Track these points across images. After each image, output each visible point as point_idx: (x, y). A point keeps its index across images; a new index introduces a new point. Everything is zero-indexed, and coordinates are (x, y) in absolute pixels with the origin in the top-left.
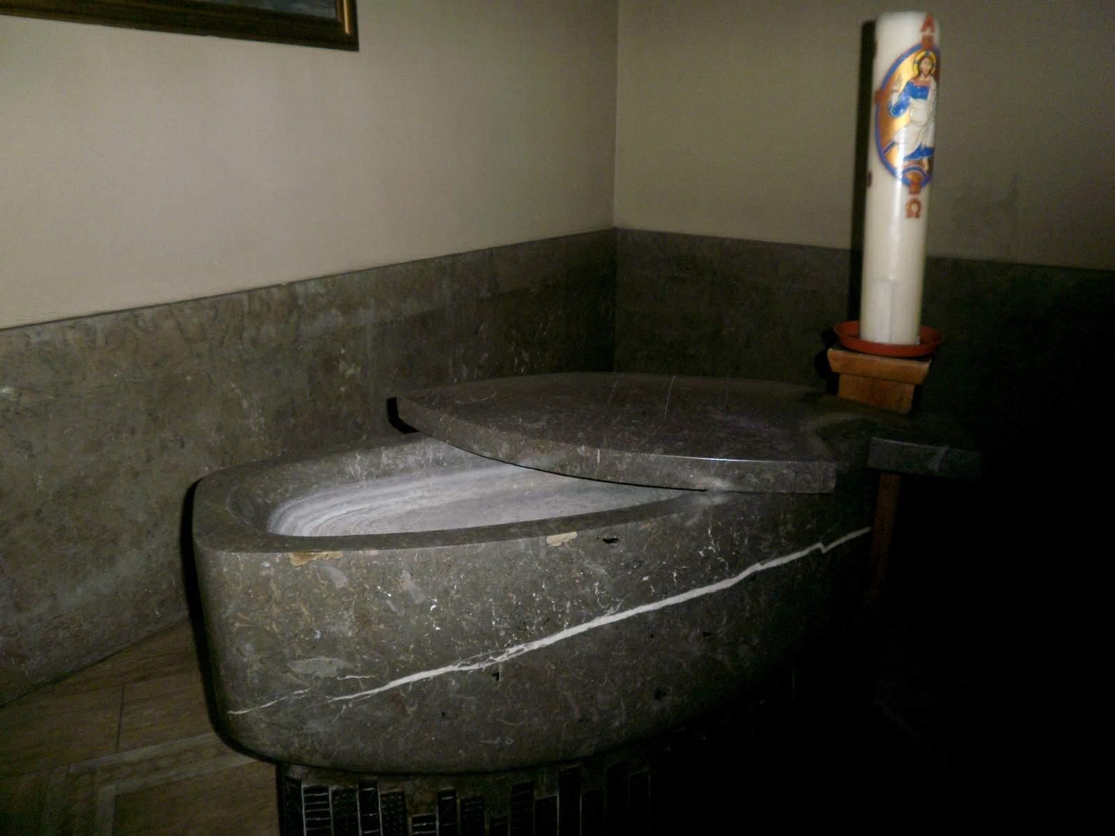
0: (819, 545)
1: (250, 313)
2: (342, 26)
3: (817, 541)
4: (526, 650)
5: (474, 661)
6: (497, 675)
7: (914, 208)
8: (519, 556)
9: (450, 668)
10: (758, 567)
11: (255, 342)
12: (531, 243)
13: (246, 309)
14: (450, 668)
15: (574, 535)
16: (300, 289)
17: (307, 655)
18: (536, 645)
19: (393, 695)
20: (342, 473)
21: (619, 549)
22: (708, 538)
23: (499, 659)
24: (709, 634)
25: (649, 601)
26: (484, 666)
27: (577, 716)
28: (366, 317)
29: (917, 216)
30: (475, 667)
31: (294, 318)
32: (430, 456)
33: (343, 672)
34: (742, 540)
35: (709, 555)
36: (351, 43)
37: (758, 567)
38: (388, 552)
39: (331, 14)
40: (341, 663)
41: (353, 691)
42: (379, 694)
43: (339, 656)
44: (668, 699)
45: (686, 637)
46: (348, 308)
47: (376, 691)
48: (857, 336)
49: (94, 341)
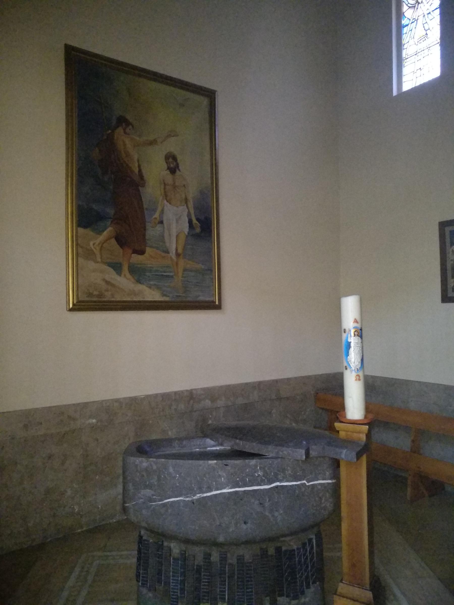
0: (305, 482)
1: (175, 399)
2: (215, 302)
3: (304, 480)
4: (202, 496)
5: (187, 497)
6: (193, 503)
7: (358, 377)
8: (200, 466)
9: (181, 498)
10: (278, 484)
11: (176, 410)
12: (296, 378)
13: (174, 398)
14: (181, 498)
15: (215, 461)
16: (194, 392)
17: (144, 489)
18: (205, 495)
19: (165, 505)
20: (171, 445)
21: (228, 468)
22: (258, 470)
23: (194, 498)
24: (262, 504)
25: (240, 487)
26: (190, 499)
27: (218, 524)
28: (221, 403)
29: (359, 380)
30: (187, 499)
31: (191, 402)
32: (198, 443)
33: (153, 495)
34: (271, 473)
35: (259, 475)
36: (217, 307)
37: (278, 484)
38: (167, 460)
39: (211, 299)
40: (152, 492)
41: (155, 502)
42: (162, 504)
43: (152, 490)
44: (249, 525)
45: (254, 503)
46: (213, 399)
47: (161, 503)
48: (345, 417)
49: (122, 407)
